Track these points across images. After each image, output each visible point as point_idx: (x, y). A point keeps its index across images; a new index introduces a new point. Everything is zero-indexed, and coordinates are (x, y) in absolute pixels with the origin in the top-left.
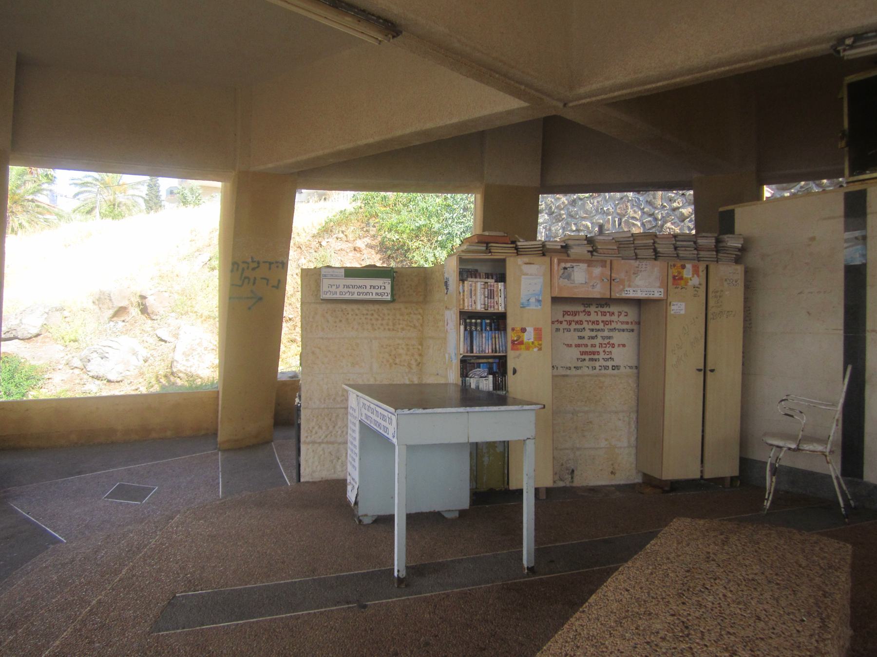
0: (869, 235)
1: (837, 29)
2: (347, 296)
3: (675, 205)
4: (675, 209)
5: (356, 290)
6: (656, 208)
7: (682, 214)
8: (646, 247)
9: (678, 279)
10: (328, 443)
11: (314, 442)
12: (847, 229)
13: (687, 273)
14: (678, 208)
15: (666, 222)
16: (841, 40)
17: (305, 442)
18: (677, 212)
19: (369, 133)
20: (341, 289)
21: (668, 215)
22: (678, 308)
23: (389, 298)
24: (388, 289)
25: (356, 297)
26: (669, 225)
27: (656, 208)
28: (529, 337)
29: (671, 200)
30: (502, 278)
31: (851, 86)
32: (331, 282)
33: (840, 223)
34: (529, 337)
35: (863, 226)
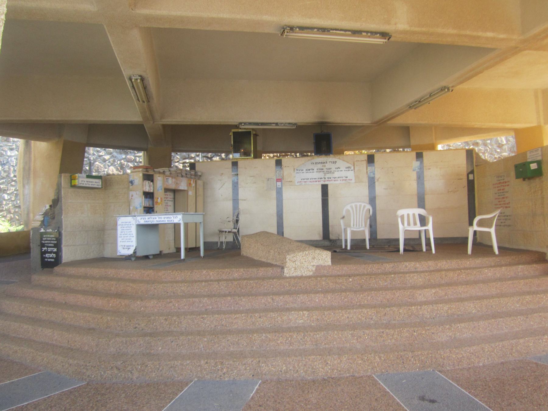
0: (239, 173)
1: (241, 121)
2: (87, 186)
3: (101, 154)
4: (100, 156)
5: (90, 183)
6: (90, 154)
7: (104, 159)
8: (179, 173)
9: (190, 184)
10: (74, 245)
11: (68, 246)
12: (233, 171)
13: (192, 182)
14: (102, 156)
15: (96, 162)
16: (241, 123)
17: (65, 246)
18: (102, 158)
19: (54, 114)
20: (85, 183)
21: (97, 158)
22: (190, 193)
23: (100, 187)
24: (101, 184)
25: (90, 186)
26: (97, 163)
27: (90, 154)
28: (159, 200)
29: (98, 151)
30: (152, 181)
31: (234, 133)
32: (83, 179)
33: (230, 170)
34: (159, 200)
35: (237, 171)
